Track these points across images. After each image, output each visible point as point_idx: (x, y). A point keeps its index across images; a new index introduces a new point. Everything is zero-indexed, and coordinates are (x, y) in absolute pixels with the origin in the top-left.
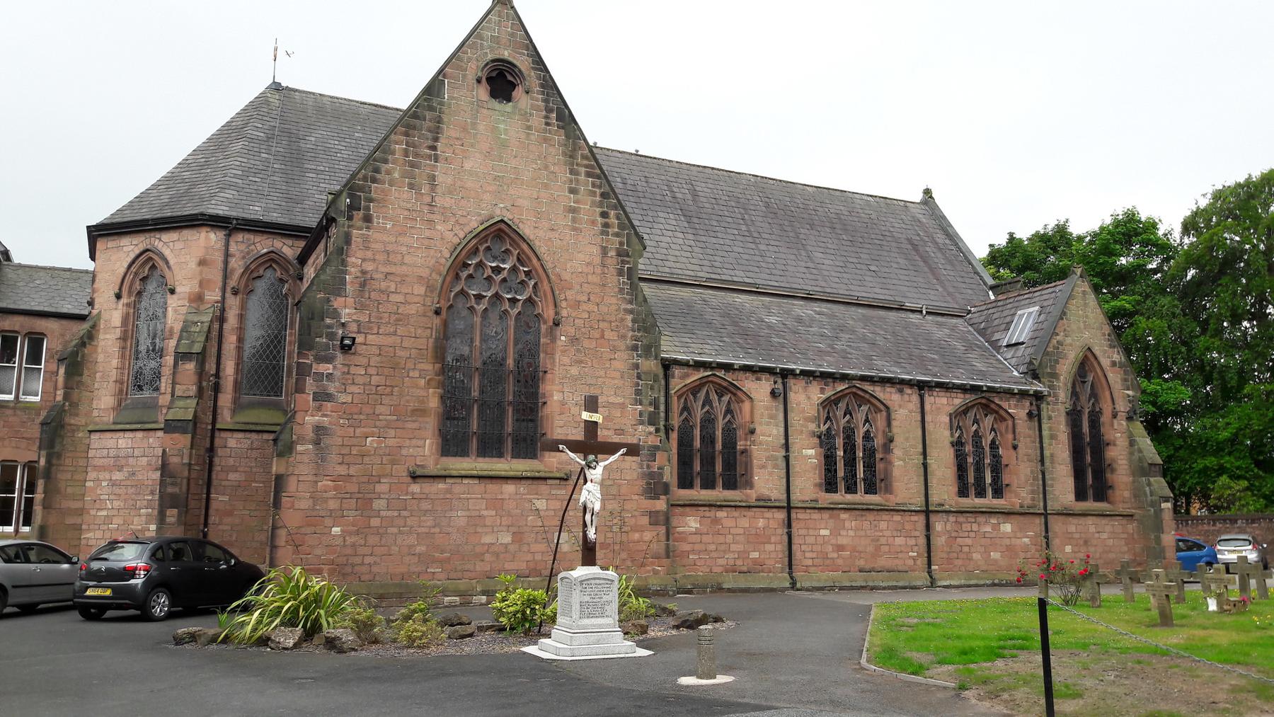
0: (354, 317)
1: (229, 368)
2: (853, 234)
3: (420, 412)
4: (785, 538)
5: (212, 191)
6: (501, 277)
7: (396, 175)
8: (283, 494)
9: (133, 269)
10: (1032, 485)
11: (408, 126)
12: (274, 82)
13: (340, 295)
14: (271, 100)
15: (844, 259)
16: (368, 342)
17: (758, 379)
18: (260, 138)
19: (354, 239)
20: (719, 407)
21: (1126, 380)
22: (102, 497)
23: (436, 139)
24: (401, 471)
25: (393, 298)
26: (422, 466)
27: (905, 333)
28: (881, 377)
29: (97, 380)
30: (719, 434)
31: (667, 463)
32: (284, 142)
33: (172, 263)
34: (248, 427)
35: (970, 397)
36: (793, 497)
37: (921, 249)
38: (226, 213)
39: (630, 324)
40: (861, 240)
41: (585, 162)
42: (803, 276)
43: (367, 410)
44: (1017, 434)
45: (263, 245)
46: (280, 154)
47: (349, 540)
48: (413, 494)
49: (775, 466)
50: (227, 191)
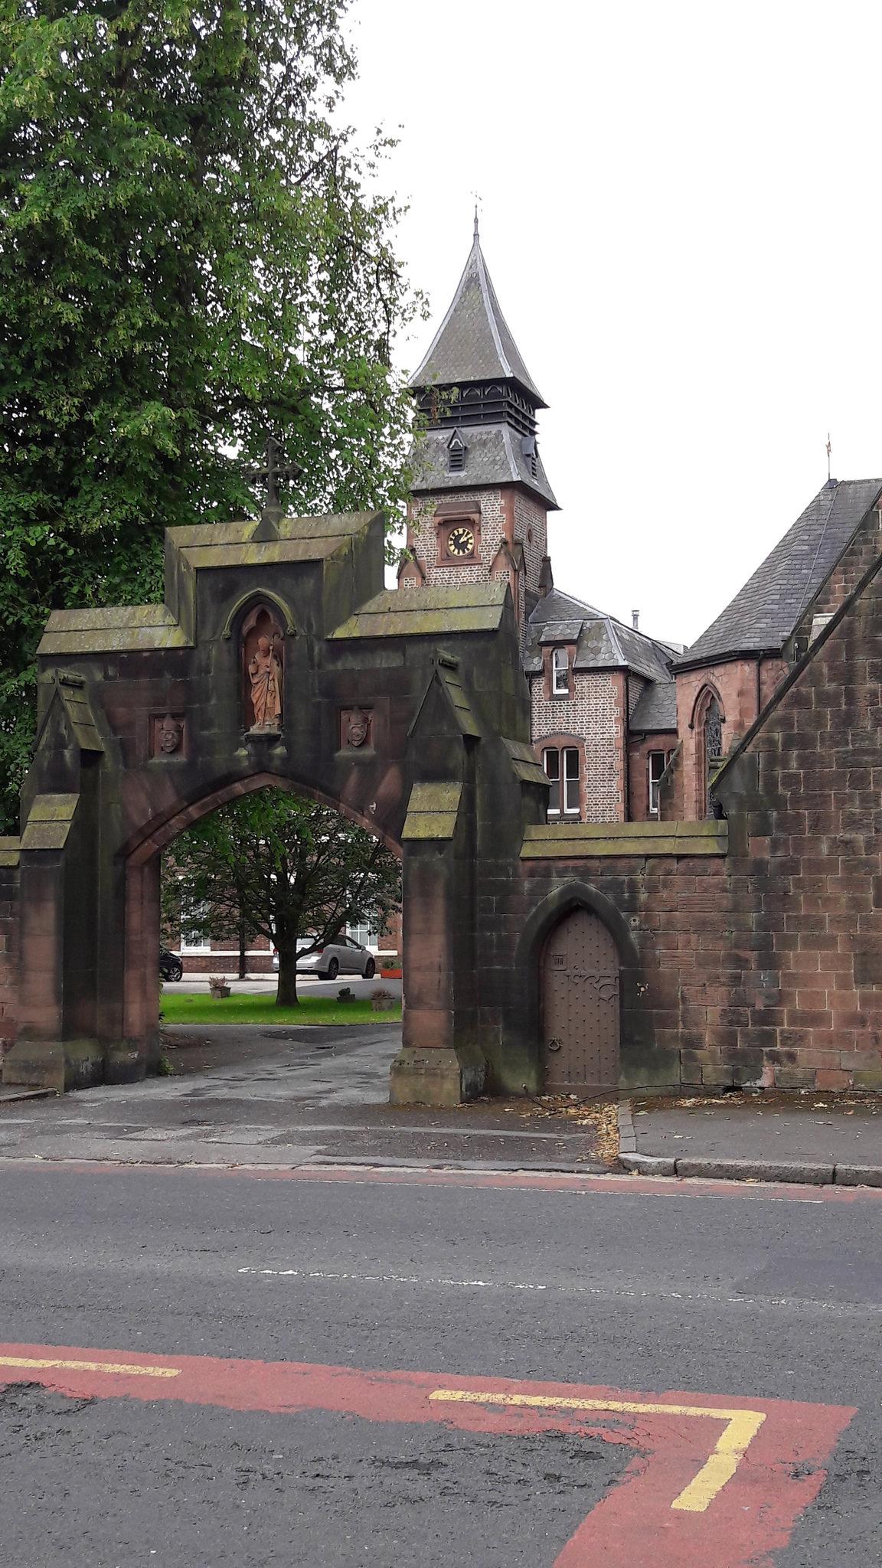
9: (699, 702)
11: (845, 564)
12: (830, 480)
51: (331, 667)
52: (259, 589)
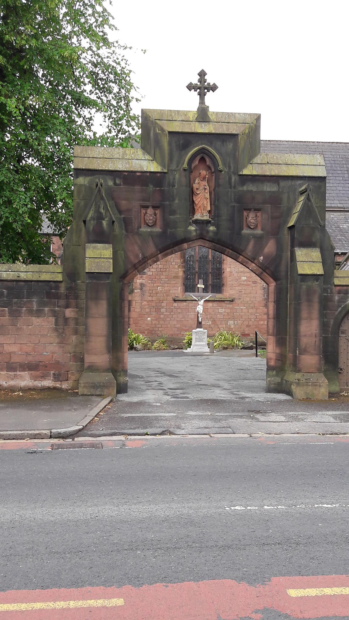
3: (176, 277)
24: (170, 298)
48: (175, 306)
51: (240, 189)
52: (204, 146)
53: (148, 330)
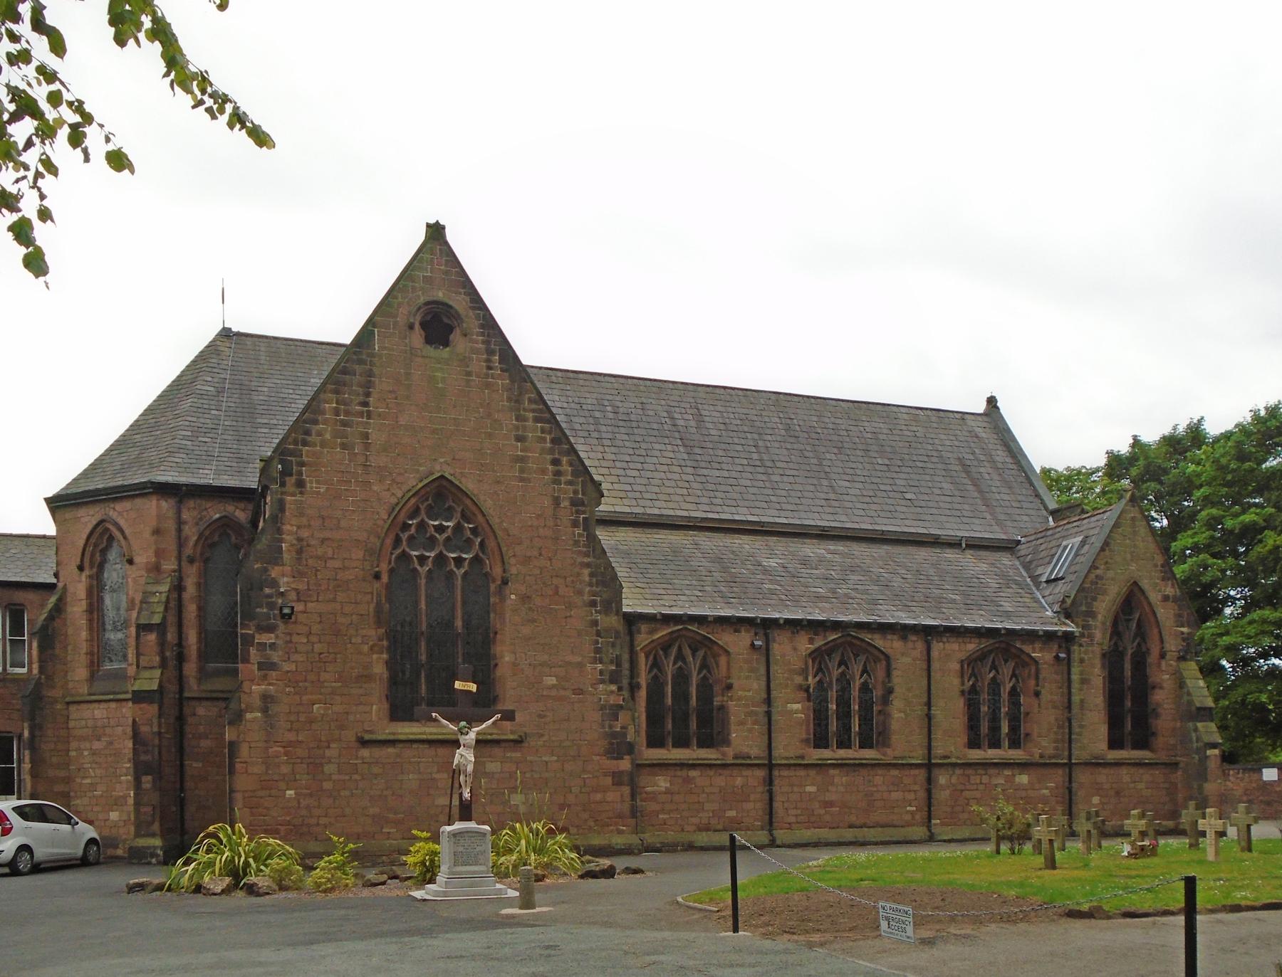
0: (293, 586)
1: (192, 637)
2: (891, 456)
3: (367, 678)
4: (766, 796)
5: (161, 456)
6: (445, 535)
7: (328, 436)
8: (238, 760)
9: (93, 540)
10: (1056, 733)
11: (337, 383)
12: (224, 328)
13: (277, 564)
14: (222, 349)
15: (875, 487)
16: (308, 611)
17: (736, 631)
18: (209, 393)
19: (287, 506)
20: (693, 664)
21: (1180, 616)
22: (86, 766)
23: (368, 395)
24: (350, 736)
25: (331, 564)
26: (371, 732)
27: (931, 572)
28: (880, 624)
29: (69, 652)
30: (693, 690)
31: (631, 722)
32: (235, 396)
33: (127, 532)
34: (214, 695)
35: (985, 643)
36: (775, 753)
37: (973, 470)
38: (176, 479)
39: (587, 579)
40: (899, 463)
41: (534, 406)
42: (820, 509)
43: (311, 677)
44: (1040, 680)
45: (215, 512)
46: (232, 409)
47: (304, 803)
48: (363, 758)
49: (755, 723)
50: (177, 455)
53: (289, 823)
